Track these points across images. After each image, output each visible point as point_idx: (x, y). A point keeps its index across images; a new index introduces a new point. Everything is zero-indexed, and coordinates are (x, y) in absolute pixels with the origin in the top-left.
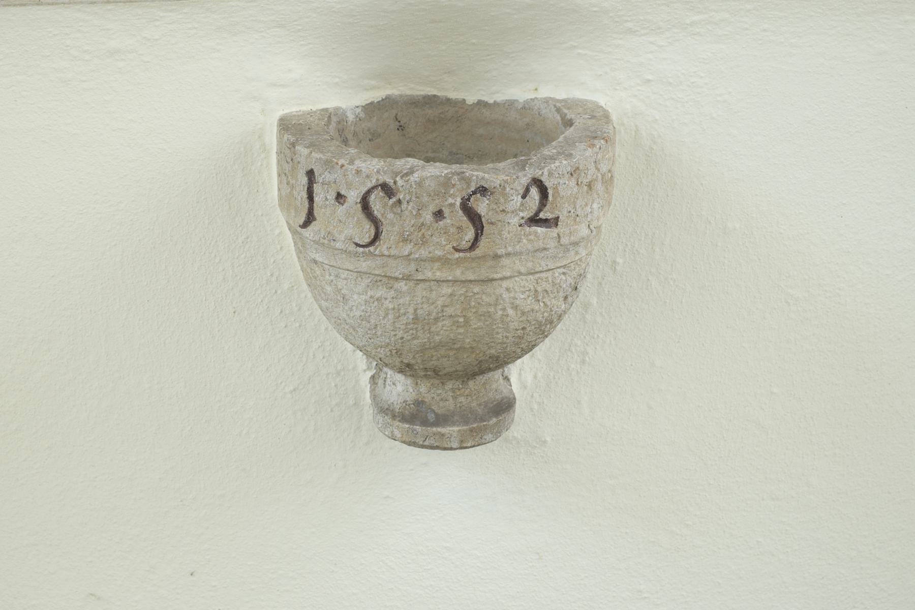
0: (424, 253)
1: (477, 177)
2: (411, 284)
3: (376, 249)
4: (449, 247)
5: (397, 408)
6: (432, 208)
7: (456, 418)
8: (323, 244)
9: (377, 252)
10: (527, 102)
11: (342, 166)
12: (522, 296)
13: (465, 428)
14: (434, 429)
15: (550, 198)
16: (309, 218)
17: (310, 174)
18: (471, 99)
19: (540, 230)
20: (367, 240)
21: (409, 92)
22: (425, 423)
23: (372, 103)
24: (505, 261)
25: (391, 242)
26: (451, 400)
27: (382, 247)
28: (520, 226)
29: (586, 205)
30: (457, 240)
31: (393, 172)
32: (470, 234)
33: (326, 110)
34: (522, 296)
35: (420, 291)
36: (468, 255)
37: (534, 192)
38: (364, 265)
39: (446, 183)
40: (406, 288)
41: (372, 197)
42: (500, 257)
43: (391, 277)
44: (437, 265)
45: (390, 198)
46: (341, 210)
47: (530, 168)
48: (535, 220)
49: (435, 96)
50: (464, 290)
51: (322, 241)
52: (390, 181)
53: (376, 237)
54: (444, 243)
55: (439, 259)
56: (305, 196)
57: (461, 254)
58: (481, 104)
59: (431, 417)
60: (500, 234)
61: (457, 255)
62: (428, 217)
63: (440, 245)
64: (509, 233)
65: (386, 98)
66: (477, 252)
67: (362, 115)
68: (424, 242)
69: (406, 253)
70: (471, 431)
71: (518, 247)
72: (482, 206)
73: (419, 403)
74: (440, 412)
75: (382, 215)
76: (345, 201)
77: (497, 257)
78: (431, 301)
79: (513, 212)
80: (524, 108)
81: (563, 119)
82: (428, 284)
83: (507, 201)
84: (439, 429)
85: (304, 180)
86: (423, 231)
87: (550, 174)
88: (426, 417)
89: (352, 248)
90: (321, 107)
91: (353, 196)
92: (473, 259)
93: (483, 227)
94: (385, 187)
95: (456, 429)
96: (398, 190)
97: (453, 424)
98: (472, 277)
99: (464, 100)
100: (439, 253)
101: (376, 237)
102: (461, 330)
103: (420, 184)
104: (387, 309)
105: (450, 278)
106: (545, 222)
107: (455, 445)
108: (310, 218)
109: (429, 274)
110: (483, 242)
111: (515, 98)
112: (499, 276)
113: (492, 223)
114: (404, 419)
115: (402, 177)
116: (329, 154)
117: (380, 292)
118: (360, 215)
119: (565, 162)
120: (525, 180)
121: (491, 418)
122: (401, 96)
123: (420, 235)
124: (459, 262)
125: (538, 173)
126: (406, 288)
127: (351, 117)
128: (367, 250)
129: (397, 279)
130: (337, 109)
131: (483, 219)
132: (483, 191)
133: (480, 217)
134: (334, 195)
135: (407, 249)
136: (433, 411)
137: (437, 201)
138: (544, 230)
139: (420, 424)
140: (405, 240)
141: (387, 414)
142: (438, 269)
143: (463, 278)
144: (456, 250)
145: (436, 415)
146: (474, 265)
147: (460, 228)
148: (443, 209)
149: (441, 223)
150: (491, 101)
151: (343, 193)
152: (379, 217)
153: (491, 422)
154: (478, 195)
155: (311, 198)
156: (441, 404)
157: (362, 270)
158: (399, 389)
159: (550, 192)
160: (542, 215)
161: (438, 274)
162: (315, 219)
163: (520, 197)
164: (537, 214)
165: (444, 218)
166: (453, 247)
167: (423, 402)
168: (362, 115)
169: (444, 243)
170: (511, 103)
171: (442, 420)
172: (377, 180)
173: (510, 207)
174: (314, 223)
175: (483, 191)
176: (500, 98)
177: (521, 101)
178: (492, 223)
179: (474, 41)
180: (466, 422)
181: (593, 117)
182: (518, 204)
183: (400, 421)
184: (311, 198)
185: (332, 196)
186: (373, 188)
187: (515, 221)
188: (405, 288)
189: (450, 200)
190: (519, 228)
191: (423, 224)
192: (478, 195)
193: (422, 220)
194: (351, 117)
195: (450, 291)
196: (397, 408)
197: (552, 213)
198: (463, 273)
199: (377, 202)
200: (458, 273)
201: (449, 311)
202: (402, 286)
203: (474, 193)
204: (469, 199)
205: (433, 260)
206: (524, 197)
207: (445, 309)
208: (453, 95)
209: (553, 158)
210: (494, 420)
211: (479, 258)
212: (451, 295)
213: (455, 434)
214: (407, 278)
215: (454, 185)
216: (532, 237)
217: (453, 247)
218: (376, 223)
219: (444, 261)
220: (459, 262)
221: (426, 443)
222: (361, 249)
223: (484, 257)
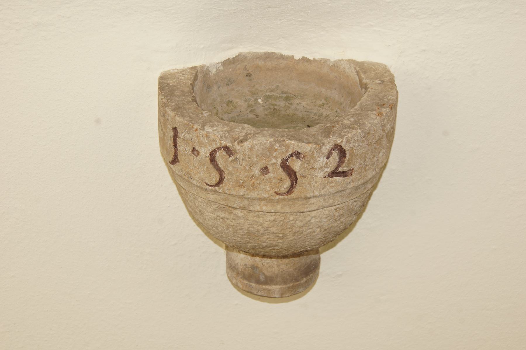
0: (254, 194)
1: (294, 145)
2: (245, 212)
3: (220, 189)
4: (272, 192)
5: (240, 268)
6: (260, 165)
7: (279, 279)
8: (184, 179)
9: (220, 191)
10: (336, 62)
11: (196, 130)
12: (325, 220)
13: (284, 286)
14: (264, 287)
15: (347, 157)
16: (175, 159)
17: (175, 129)
18: (297, 57)
19: (337, 179)
20: (214, 183)
21: (255, 51)
22: (258, 282)
23: (229, 59)
24: (313, 200)
25: (230, 186)
26: (276, 267)
27: (225, 187)
28: (325, 177)
29: (374, 156)
30: (278, 187)
31: (233, 138)
32: (287, 184)
33: (194, 68)
34: (325, 220)
35: (250, 216)
36: (286, 197)
37: (335, 155)
38: (212, 197)
39: (271, 149)
40: (242, 214)
41: (218, 155)
42: (310, 198)
43: (231, 207)
44: (263, 202)
45: (230, 156)
46: (196, 160)
47: (333, 135)
48: (335, 173)
49: (273, 53)
50: (283, 218)
51: (184, 177)
52: (229, 145)
53: (220, 181)
54: (269, 189)
55: (264, 199)
56: (172, 144)
57: (281, 197)
58: (304, 60)
59: (262, 278)
60: (309, 183)
61: (278, 197)
62: (256, 172)
63: (266, 189)
64: (316, 182)
65: (239, 55)
66: (293, 195)
67: (221, 68)
68: (254, 188)
69: (242, 194)
70: (289, 288)
71: (322, 192)
72: (296, 165)
73: (254, 267)
74: (268, 274)
75: (224, 167)
76: (198, 154)
77: (306, 198)
78: (259, 224)
79: (319, 169)
80: (334, 65)
81: (360, 81)
82: (257, 213)
83: (316, 161)
84: (268, 287)
85: (172, 134)
86: (253, 180)
87: (348, 141)
88: (259, 277)
89: (204, 186)
90: (191, 65)
91: (205, 152)
92: (290, 200)
93: (297, 179)
94: (226, 148)
95: (278, 287)
96: (235, 152)
97: (276, 284)
98: (288, 211)
99: (293, 56)
100: (265, 196)
101: (220, 181)
102: (280, 241)
103: (251, 149)
104: (229, 225)
105: (273, 211)
106: (344, 174)
107: (277, 296)
108: (175, 160)
109: (258, 208)
110: (297, 189)
111: (328, 58)
112: (308, 210)
113: (304, 177)
114: (244, 277)
115: (238, 143)
116: (188, 118)
117: (223, 215)
118: (211, 166)
119: (359, 131)
120: (329, 147)
121: (302, 278)
122: (249, 53)
123: (251, 183)
124: (278, 201)
125: (339, 141)
126: (242, 214)
127: (213, 71)
128: (214, 188)
129: (235, 208)
130: (202, 67)
131: (297, 174)
132: (297, 154)
133: (295, 173)
134: (191, 149)
135: (242, 192)
136: (264, 274)
137: (264, 161)
138: (342, 178)
139: (251, 282)
140: (241, 186)
141: (234, 271)
142: (265, 205)
143: (282, 211)
144: (278, 194)
145: (266, 277)
146: (290, 203)
147: (281, 180)
148: (268, 166)
149: (267, 176)
150: (311, 58)
151: (197, 148)
152: (222, 168)
153: (302, 282)
154: (294, 157)
155: (175, 145)
156: (269, 269)
157: (212, 200)
158: (242, 259)
159: (348, 153)
160: (340, 169)
161: (264, 208)
162: (178, 161)
163: (325, 158)
164: (336, 169)
165: (269, 172)
166: (275, 192)
167: (257, 267)
168: (221, 68)
169: (269, 189)
170: (323, 62)
171: (269, 280)
172: (221, 144)
173: (316, 166)
174: (178, 163)
175: (297, 154)
176: (318, 57)
177: (332, 60)
178: (304, 177)
179: (300, 19)
180: (285, 283)
181: (382, 82)
182: (324, 163)
183: (241, 278)
184: (175, 145)
185: (189, 149)
186: (218, 148)
187: (321, 174)
188: (240, 214)
189: (274, 161)
190: (324, 179)
191: (253, 176)
192: (294, 157)
193: (252, 173)
194: (213, 71)
195: (272, 218)
196: (240, 268)
197: (348, 167)
198: (282, 208)
199: (220, 156)
200: (279, 207)
201: (273, 230)
202: (239, 213)
203: (291, 156)
204: (287, 160)
205: (260, 199)
206: (328, 158)
207: (269, 229)
208: (285, 53)
209: (351, 127)
210: (305, 279)
211: (294, 199)
212: (273, 221)
213: (277, 290)
214: (243, 208)
215: (276, 150)
216: (333, 184)
217: (275, 192)
218: (221, 172)
219: (269, 201)
220: (278, 201)
221: (259, 294)
222: (210, 188)
223: (298, 199)
